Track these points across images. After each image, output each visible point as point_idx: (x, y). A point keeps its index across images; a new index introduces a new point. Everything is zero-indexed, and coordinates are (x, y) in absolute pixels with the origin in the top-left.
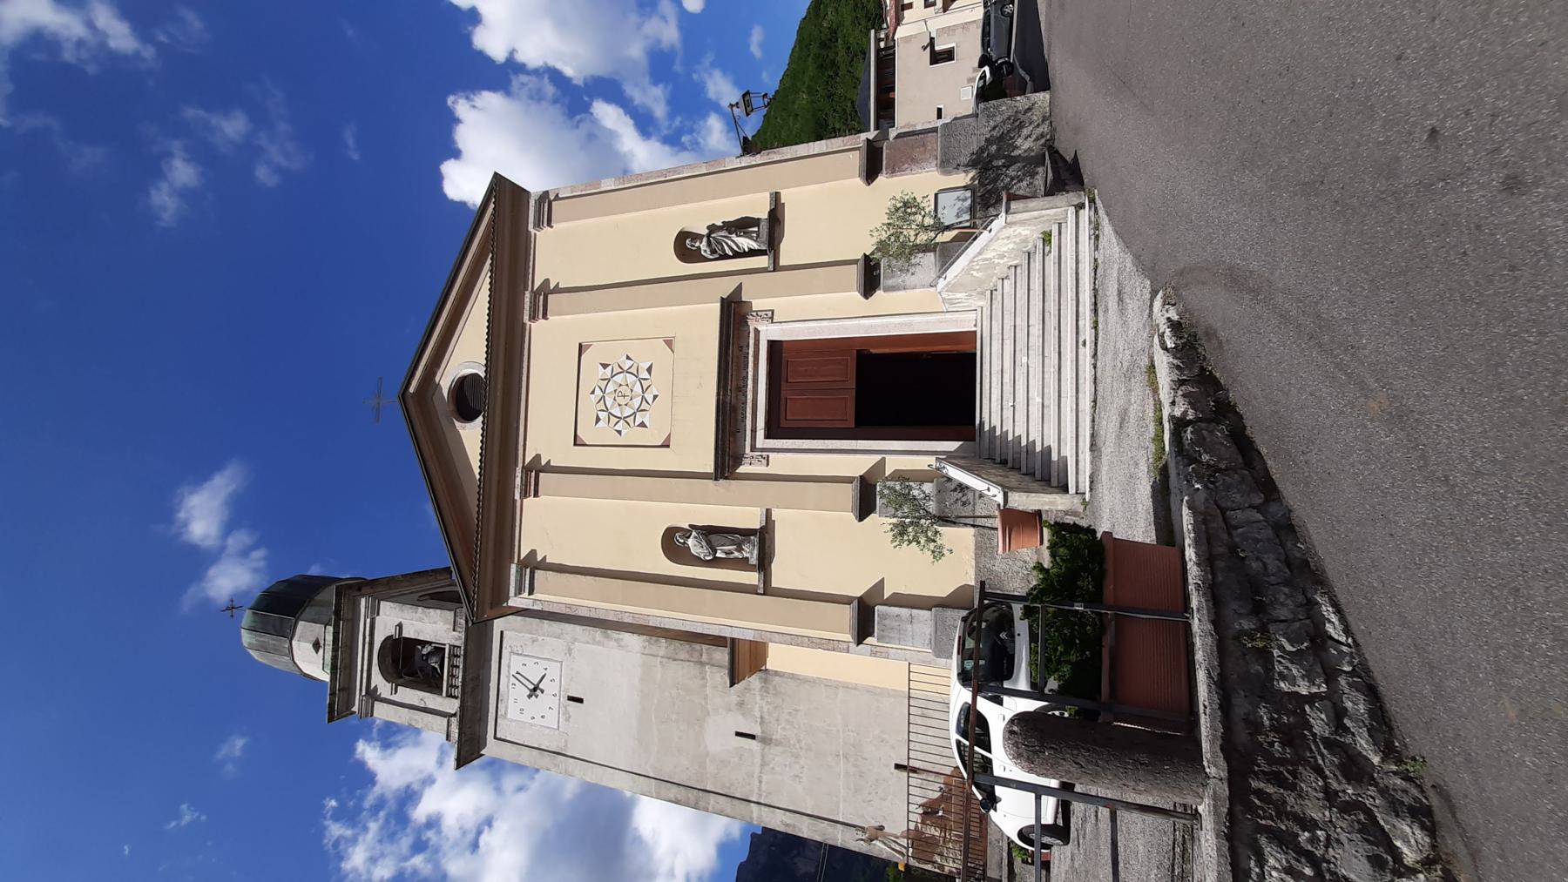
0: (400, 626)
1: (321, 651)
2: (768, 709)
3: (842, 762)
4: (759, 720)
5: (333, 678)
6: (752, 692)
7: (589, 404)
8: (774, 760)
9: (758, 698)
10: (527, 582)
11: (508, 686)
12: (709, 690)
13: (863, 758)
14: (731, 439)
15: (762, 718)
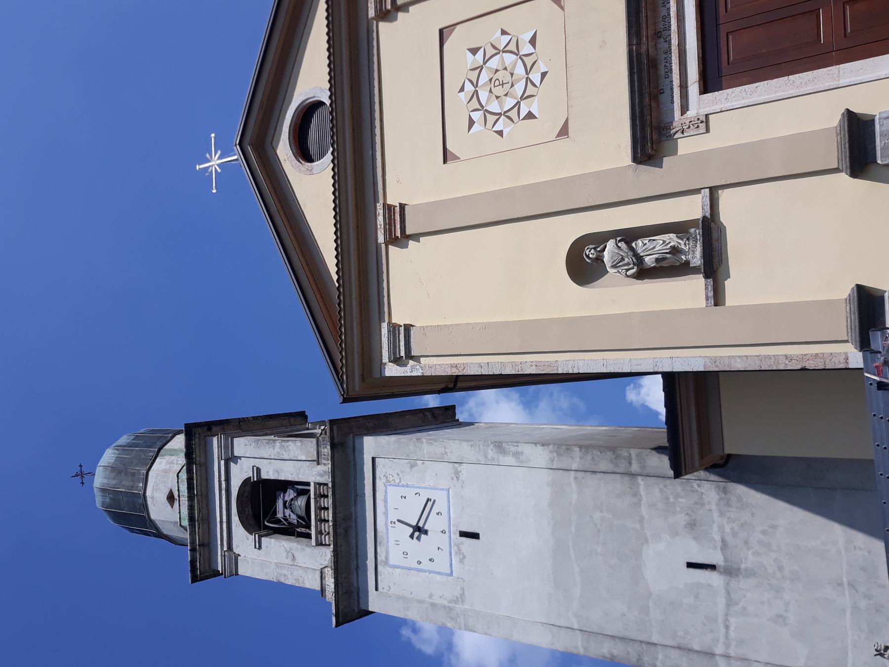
0: (259, 470)
1: (176, 504)
2: (732, 529)
3: (847, 593)
4: (719, 544)
5: (192, 533)
6: (707, 507)
7: (458, 103)
8: (745, 596)
9: (716, 514)
10: (402, 343)
11: (386, 525)
12: (644, 511)
13: (879, 586)
14: (653, 104)
15: (723, 541)
